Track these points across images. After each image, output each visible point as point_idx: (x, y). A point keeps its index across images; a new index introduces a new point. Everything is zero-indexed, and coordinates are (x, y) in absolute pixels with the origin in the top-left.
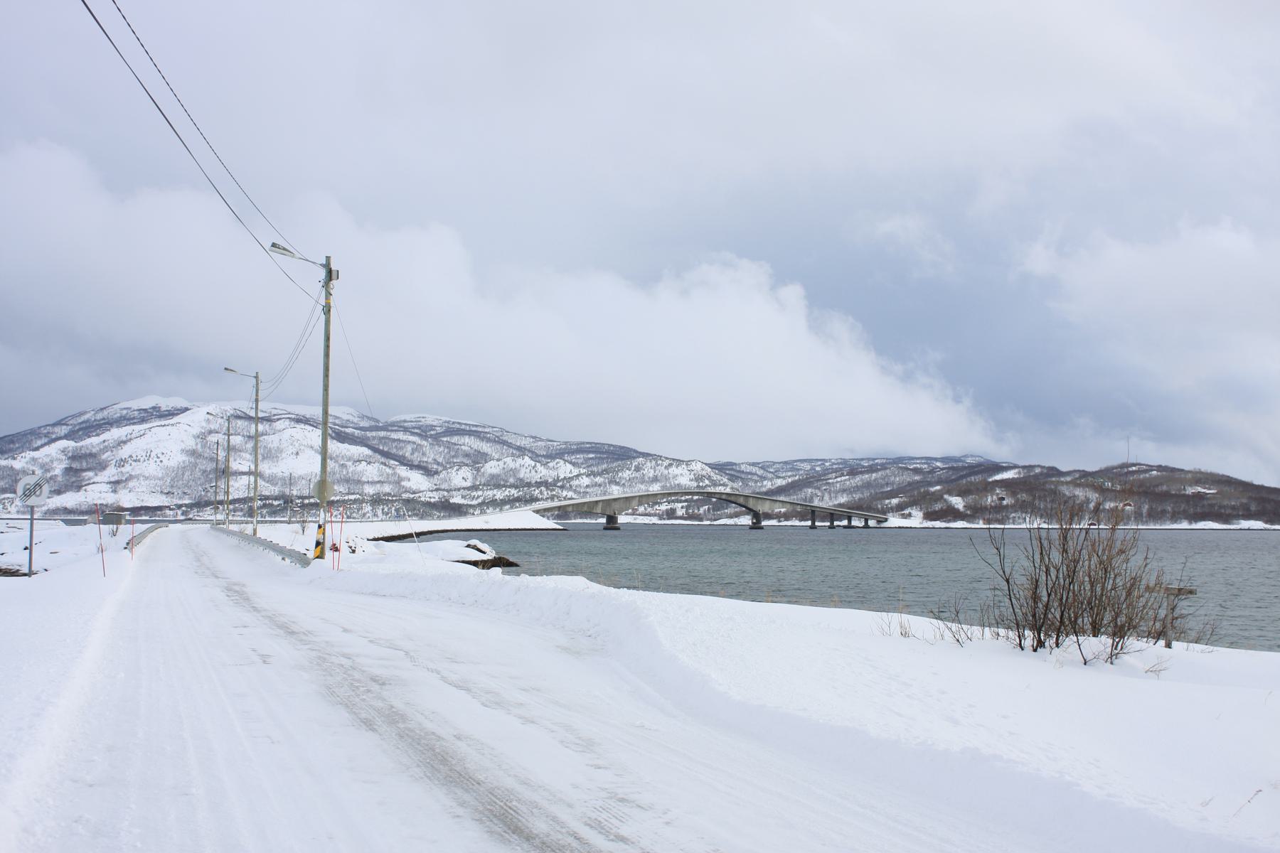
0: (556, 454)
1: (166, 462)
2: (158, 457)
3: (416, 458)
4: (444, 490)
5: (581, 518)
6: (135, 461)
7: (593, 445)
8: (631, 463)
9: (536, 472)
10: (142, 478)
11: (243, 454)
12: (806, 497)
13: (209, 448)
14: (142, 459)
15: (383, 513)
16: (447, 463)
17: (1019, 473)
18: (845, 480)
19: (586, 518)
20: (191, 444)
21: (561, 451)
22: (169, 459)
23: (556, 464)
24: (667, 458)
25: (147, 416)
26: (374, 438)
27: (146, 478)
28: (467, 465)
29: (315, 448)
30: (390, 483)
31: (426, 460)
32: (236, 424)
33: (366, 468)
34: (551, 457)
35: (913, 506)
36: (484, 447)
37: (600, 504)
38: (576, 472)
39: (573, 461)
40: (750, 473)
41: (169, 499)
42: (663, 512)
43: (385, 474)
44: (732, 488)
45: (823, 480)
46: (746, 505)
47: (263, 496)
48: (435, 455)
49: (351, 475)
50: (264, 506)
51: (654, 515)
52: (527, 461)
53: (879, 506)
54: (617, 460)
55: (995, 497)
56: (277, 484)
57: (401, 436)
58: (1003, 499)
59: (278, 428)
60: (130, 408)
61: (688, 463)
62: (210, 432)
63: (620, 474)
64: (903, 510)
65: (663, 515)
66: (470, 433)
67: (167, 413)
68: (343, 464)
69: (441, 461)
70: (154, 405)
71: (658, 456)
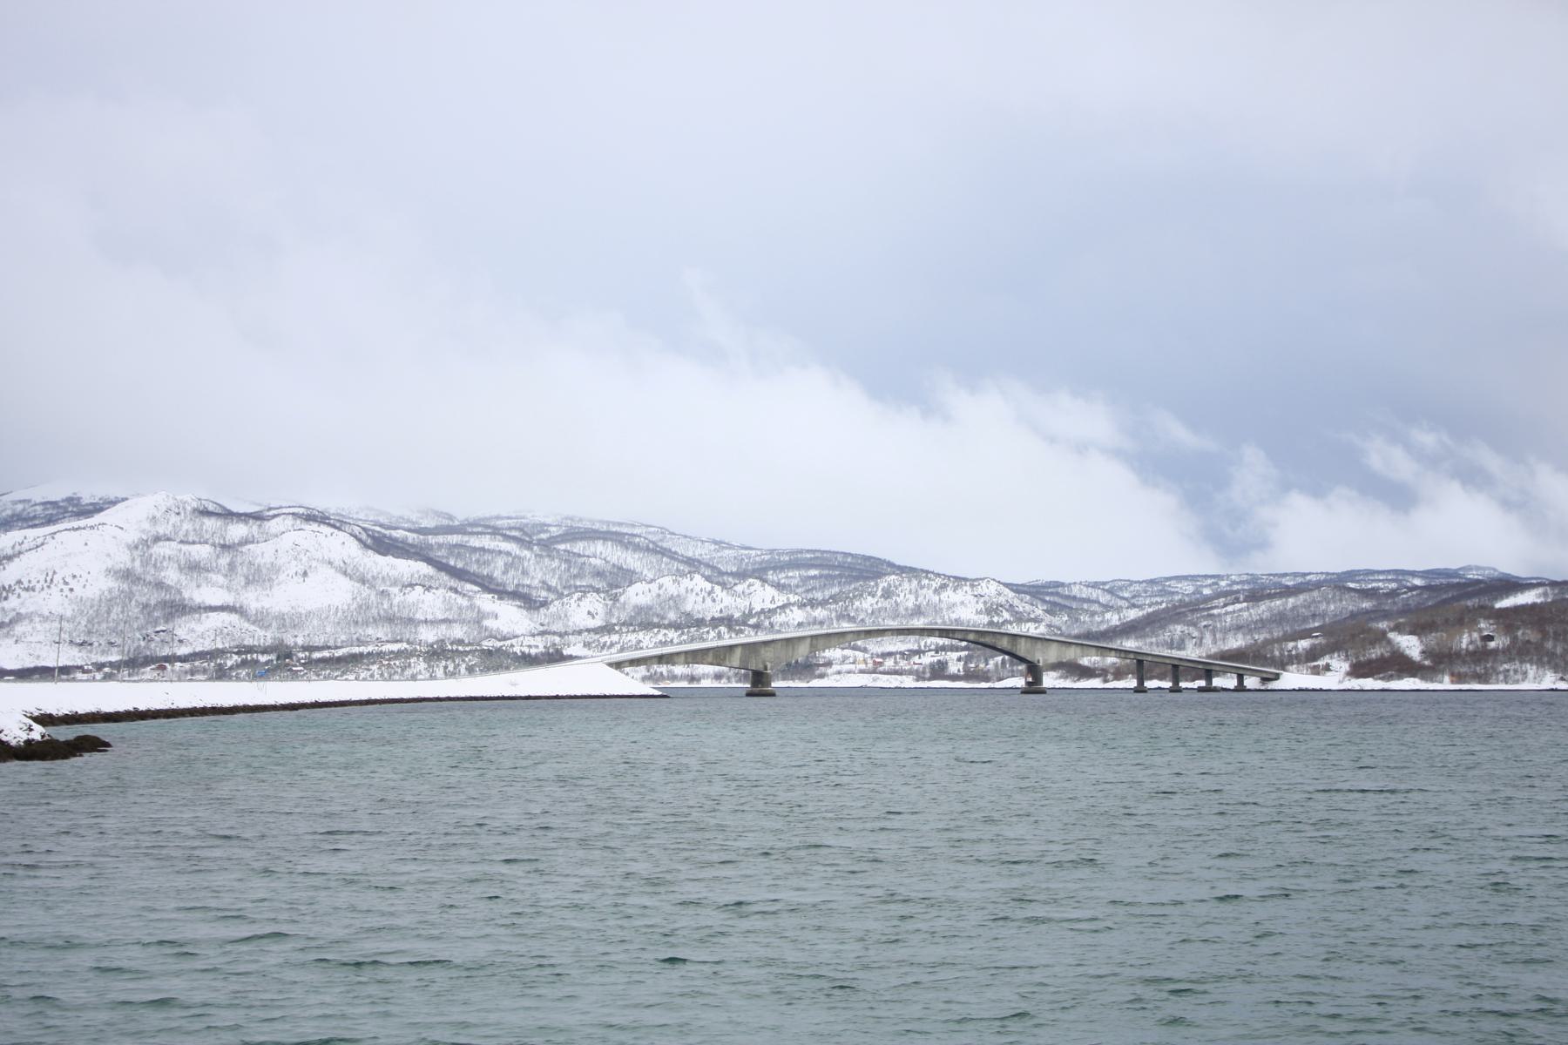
0: (754, 571)
1: (78, 591)
2: (66, 583)
3: (511, 580)
4: (554, 633)
5: (784, 679)
6: (27, 589)
7: (818, 555)
8: (877, 585)
9: (714, 601)
10: (37, 619)
11: (213, 576)
12: (1172, 640)
13: (155, 565)
14: (38, 587)
15: (445, 673)
16: (565, 588)
17: (1545, 594)
18: (1240, 610)
19: (793, 679)
20: (123, 559)
21: (764, 565)
22: (84, 586)
23: (749, 586)
24: (938, 575)
25: (56, 515)
26: (440, 546)
27: (45, 619)
28: (598, 591)
29: (336, 563)
30: (463, 622)
31: (528, 583)
32: (201, 525)
33: (422, 597)
34: (742, 575)
35: (1333, 652)
36: (629, 560)
37: (738, 652)
38: (781, 599)
39: (782, 581)
40: (1088, 600)
41: (84, 654)
42: (924, 668)
43: (455, 608)
44: (1049, 626)
45: (1204, 609)
46: (1014, 651)
47: (244, 647)
48: (545, 574)
49: (396, 609)
50: (244, 663)
51: (910, 672)
52: (699, 582)
53: (1277, 653)
54: (857, 579)
55: (1475, 635)
56: (270, 625)
57: (486, 542)
58: (1490, 638)
59: (273, 531)
60: (29, 501)
61: (973, 583)
62: (157, 539)
63: (857, 603)
64: (1315, 659)
65: (924, 672)
66: (605, 536)
67: (91, 508)
68: (383, 591)
69: (554, 584)
70: (69, 494)
71: (922, 571)
